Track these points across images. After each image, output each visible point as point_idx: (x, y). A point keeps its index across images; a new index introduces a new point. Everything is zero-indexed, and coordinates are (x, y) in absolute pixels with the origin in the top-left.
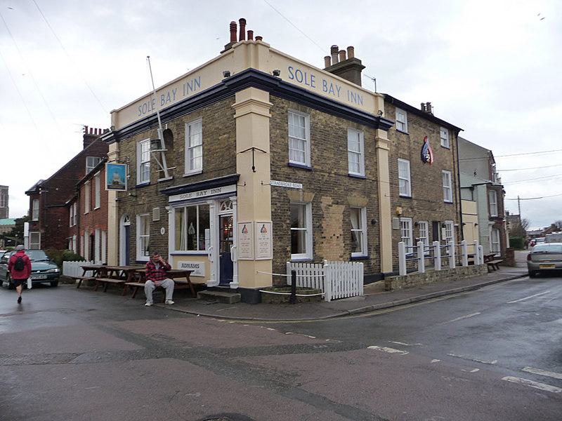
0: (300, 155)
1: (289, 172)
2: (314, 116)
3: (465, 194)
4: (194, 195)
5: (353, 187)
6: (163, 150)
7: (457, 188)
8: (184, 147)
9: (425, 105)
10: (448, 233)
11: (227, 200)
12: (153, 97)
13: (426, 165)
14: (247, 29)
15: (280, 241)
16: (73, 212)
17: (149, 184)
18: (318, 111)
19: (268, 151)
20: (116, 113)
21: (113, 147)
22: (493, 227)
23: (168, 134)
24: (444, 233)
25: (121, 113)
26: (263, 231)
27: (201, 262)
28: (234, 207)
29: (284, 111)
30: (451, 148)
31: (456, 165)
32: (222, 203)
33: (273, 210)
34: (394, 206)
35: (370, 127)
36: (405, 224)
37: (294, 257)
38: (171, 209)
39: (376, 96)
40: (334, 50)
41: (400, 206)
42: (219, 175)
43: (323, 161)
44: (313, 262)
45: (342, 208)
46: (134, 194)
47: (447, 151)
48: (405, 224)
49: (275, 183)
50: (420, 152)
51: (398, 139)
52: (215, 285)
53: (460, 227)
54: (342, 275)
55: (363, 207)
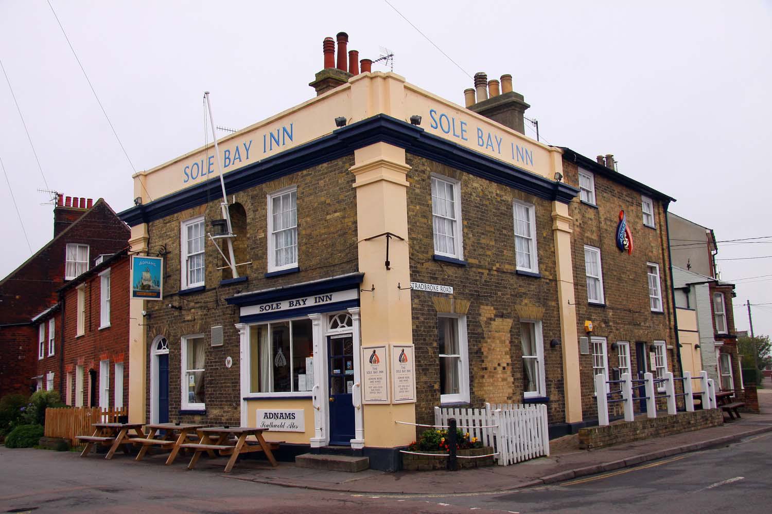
0: (450, 244)
1: (435, 268)
2: (465, 184)
3: (680, 299)
4: (285, 306)
5: (523, 290)
6: (229, 236)
7: (669, 289)
8: (265, 231)
9: (605, 159)
10: (660, 360)
11: (341, 312)
12: (210, 153)
13: (624, 255)
14: (350, 47)
15: (425, 374)
16: (48, 334)
17: (201, 290)
18: (471, 176)
19: (405, 236)
20: (142, 177)
21: (138, 232)
22: (722, 350)
23: (237, 210)
24: (653, 361)
25: (152, 178)
26: (403, 358)
27: (298, 410)
28: (355, 324)
29: (425, 176)
30: (658, 227)
31: (666, 254)
32: (331, 317)
33: (415, 327)
34: (580, 320)
35: (543, 198)
36: (594, 347)
37: (445, 399)
38: (244, 328)
39: (550, 151)
40: (480, 79)
41: (589, 319)
42: (327, 275)
43: (480, 251)
44: (471, 406)
45: (509, 323)
46: (176, 304)
47: (652, 233)
48: (594, 347)
49: (419, 286)
50: (613, 235)
51: (583, 216)
52: (323, 445)
53: (675, 350)
54: (521, 425)
55: (538, 322)
